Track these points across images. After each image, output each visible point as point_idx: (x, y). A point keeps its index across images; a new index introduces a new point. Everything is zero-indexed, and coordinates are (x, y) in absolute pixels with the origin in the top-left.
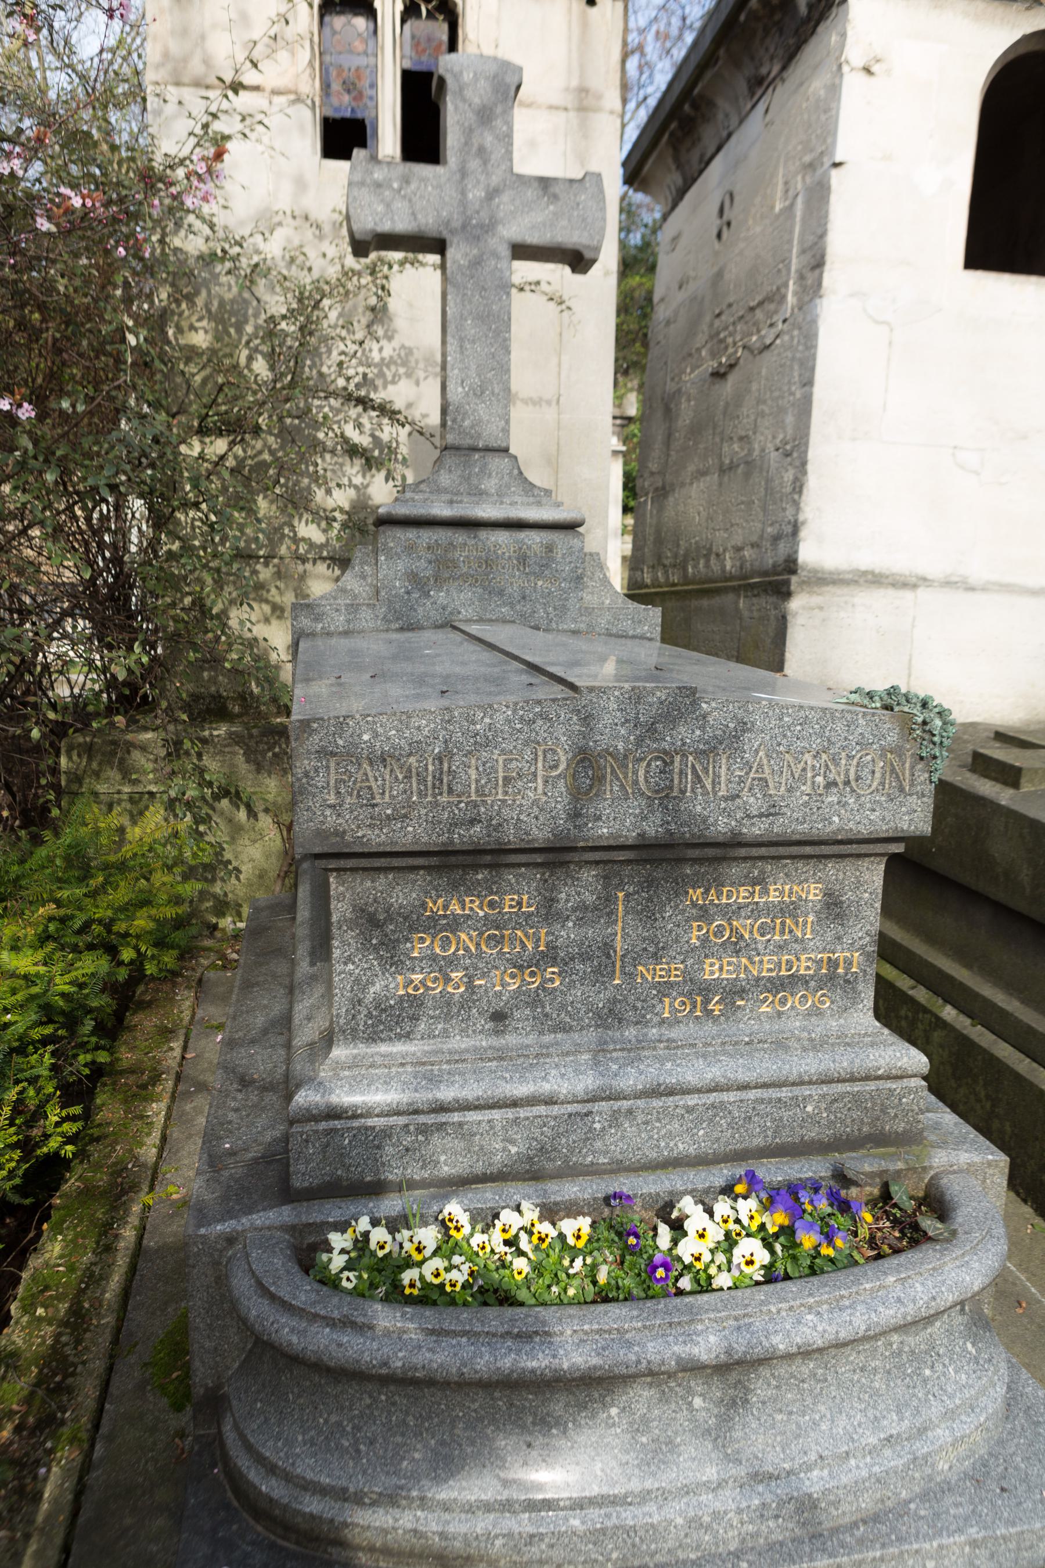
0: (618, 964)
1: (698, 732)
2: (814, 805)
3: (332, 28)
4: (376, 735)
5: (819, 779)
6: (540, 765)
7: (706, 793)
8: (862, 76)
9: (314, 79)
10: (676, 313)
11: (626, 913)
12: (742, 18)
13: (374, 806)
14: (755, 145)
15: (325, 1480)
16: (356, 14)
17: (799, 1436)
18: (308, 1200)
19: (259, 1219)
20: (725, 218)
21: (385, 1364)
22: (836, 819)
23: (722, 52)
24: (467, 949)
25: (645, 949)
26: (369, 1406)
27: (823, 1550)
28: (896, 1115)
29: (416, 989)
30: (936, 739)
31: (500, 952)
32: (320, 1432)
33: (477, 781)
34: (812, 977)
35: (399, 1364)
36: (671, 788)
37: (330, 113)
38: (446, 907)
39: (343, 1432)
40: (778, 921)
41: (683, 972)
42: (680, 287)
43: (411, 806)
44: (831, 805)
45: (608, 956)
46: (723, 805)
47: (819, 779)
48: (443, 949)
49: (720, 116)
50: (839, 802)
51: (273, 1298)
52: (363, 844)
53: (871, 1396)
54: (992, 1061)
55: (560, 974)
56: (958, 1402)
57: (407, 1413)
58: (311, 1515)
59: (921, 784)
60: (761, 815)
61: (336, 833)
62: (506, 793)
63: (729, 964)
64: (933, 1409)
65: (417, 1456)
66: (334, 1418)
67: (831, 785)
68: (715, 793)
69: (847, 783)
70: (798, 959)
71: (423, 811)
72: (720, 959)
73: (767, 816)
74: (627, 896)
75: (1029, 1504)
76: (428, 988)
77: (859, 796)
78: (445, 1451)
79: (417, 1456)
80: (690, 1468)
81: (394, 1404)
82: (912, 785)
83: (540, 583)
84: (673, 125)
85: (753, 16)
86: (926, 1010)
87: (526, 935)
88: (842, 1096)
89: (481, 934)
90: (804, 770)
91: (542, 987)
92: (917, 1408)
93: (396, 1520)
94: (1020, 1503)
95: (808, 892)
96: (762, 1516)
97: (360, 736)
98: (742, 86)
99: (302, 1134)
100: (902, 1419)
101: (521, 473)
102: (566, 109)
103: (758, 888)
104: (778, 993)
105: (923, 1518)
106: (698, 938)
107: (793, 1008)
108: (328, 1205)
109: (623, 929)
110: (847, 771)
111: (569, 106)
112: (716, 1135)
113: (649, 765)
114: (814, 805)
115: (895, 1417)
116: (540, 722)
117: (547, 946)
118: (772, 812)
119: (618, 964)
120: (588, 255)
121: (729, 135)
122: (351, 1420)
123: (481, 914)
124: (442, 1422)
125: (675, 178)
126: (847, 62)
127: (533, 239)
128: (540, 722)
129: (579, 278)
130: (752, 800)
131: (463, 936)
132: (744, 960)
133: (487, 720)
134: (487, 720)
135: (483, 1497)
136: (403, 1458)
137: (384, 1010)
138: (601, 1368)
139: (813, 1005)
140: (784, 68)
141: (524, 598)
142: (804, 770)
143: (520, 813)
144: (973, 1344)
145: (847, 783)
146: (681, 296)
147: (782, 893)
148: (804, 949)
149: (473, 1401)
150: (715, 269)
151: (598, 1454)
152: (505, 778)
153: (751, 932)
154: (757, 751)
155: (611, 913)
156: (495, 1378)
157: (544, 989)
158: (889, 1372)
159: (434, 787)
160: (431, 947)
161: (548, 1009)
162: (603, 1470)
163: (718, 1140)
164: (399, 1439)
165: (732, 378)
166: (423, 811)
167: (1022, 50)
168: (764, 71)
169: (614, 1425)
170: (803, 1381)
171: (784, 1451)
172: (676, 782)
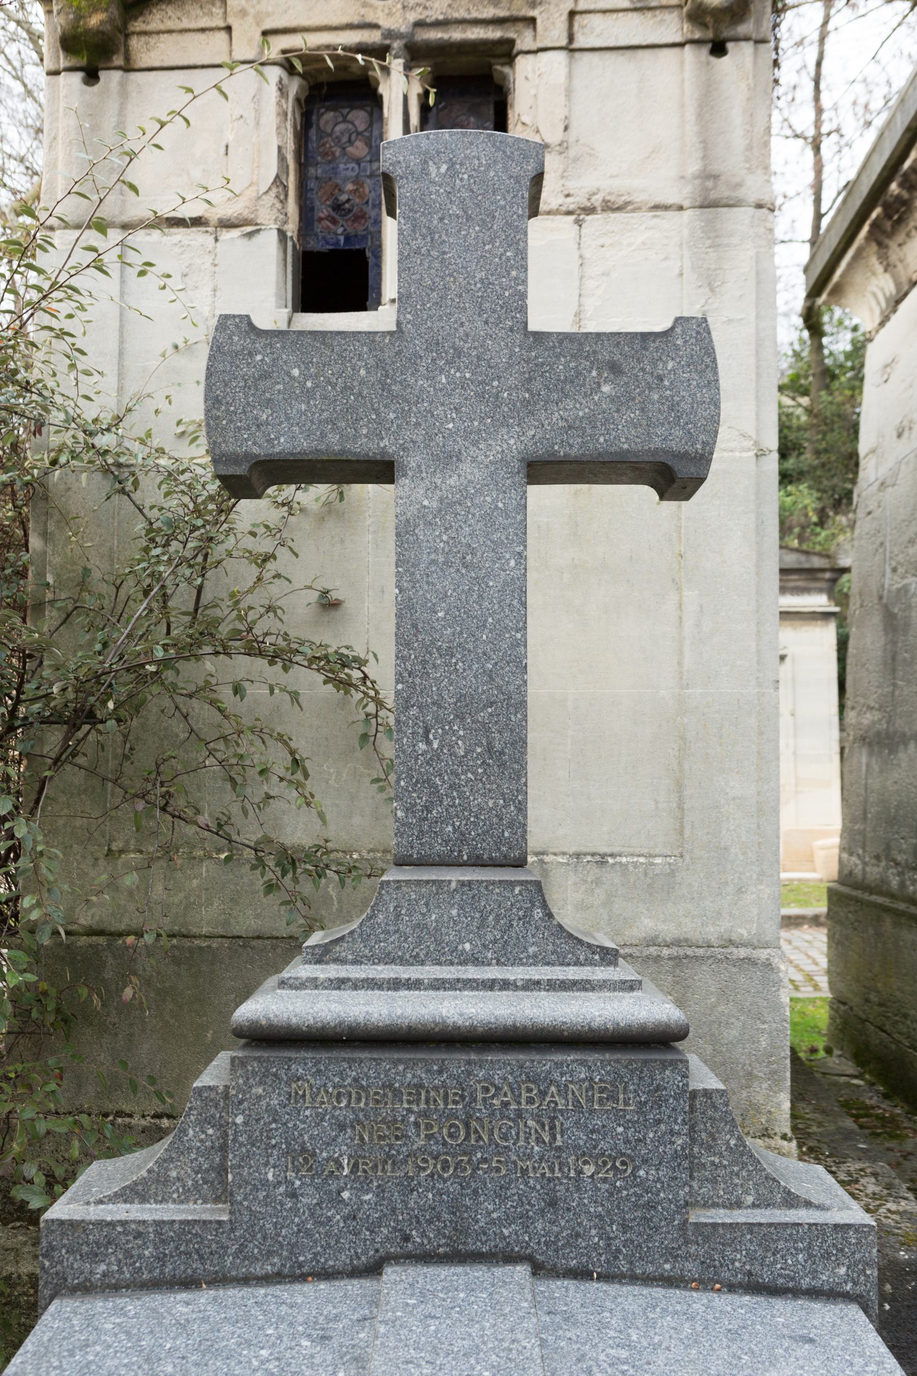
3: (318, 128)
9: (284, 202)
10: (895, 473)
16: (352, 108)
37: (315, 245)
42: (899, 436)
83: (589, 1170)
84: (876, 212)
101: (550, 916)
111: (686, 204)
120: (683, 470)
141: (553, 1203)
146: (902, 448)
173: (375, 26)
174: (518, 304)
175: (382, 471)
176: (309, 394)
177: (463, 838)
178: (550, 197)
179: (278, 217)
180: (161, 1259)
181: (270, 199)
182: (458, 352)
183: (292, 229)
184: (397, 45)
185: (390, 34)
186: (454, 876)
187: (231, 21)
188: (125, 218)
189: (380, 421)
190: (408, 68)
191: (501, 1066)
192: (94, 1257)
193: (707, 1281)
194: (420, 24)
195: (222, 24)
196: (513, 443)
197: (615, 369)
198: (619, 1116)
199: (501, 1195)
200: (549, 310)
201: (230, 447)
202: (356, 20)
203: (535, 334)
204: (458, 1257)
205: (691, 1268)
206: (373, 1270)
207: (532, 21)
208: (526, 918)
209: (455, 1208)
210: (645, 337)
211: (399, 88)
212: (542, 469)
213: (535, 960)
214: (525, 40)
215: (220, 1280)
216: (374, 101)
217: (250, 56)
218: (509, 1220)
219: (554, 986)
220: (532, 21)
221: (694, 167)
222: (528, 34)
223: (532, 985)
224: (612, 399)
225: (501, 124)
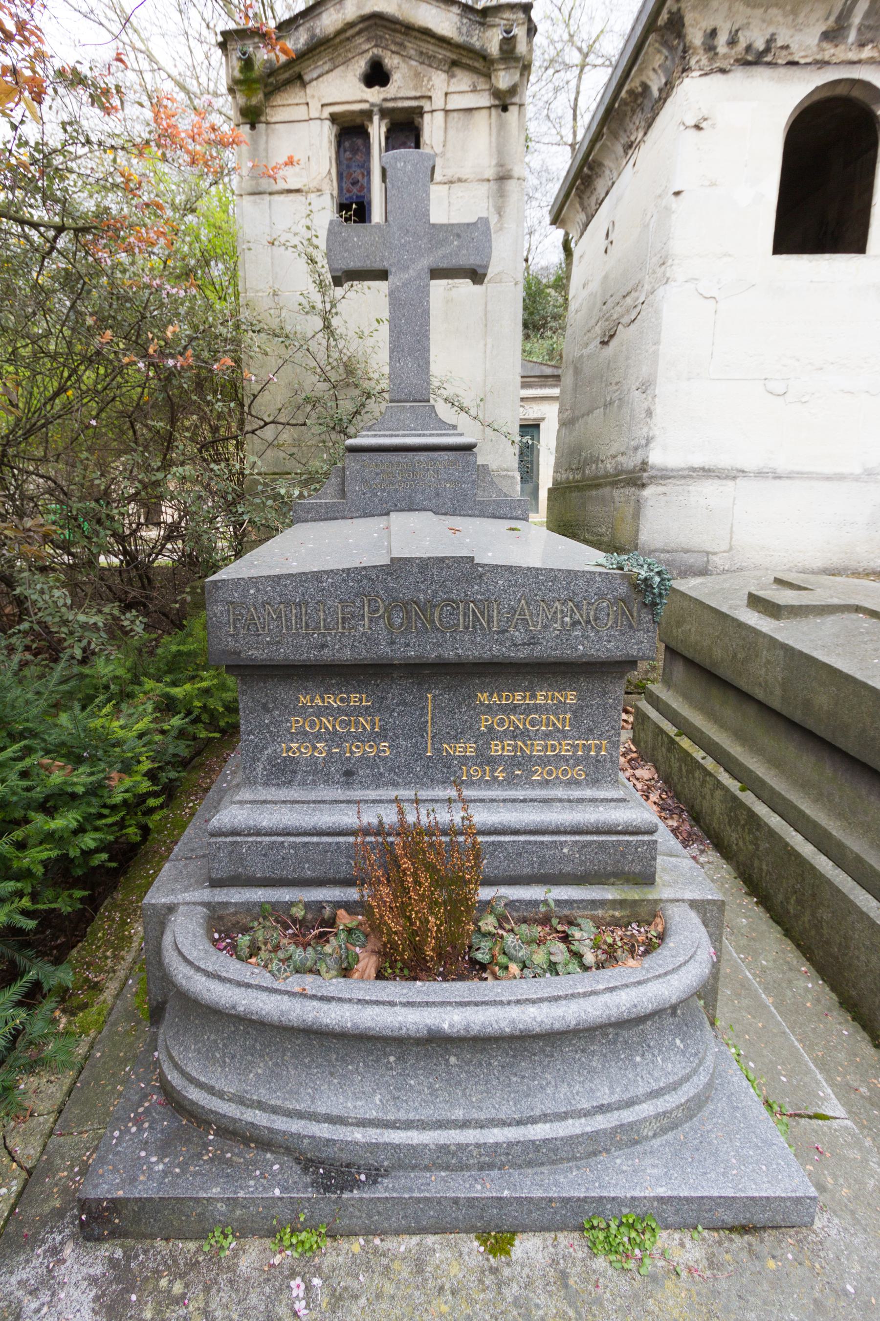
0: (430, 742)
1: (476, 587)
2: (564, 638)
4: (258, 590)
5: (567, 619)
6: (366, 609)
7: (483, 629)
8: (693, 132)
10: (581, 305)
11: (434, 708)
12: (616, 105)
13: (259, 635)
14: (629, 187)
15: (203, 1079)
17: (529, 1095)
18: (221, 887)
19: (188, 897)
20: (610, 239)
21: (234, 1007)
22: (581, 647)
23: (605, 130)
24: (326, 728)
25: (448, 733)
26: (233, 1032)
27: (540, 1186)
28: (633, 860)
29: (294, 753)
30: (656, 591)
31: (348, 731)
32: (204, 1045)
33: (325, 620)
34: (571, 757)
35: (242, 1009)
36: (458, 625)
38: (312, 701)
39: (218, 1049)
40: (544, 717)
41: (476, 750)
43: (282, 636)
44: (576, 637)
45: (423, 737)
46: (496, 637)
47: (567, 619)
48: (311, 728)
49: (607, 172)
50: (582, 636)
51: (180, 953)
52: (252, 660)
53: (589, 1072)
54: (752, 816)
55: (389, 747)
56: (662, 1085)
57: (256, 1041)
58: (192, 1100)
59: (646, 623)
60: (524, 644)
61: (235, 653)
62: (344, 628)
63: (509, 745)
64: (640, 1089)
65: (259, 1071)
66: (213, 1037)
67: (575, 623)
68: (490, 629)
69: (588, 622)
70: (560, 744)
71: (290, 639)
72: (502, 742)
73: (529, 645)
74: (434, 697)
75: (713, 1175)
76: (302, 753)
77: (598, 631)
78: (278, 1070)
79: (259, 1071)
80: (443, 1108)
81: (248, 1033)
82: (639, 623)
85: (624, 103)
86: (710, 774)
87: (366, 721)
88: (591, 843)
89: (335, 719)
90: (555, 613)
91: (377, 755)
92: (626, 1086)
93: (242, 1114)
94: (706, 1173)
95: (566, 698)
96: (496, 1152)
97: (248, 591)
98: (619, 149)
99: (216, 843)
100: (612, 1093)
102: (489, 180)
103: (528, 694)
104: (546, 766)
105: (624, 1172)
106: (486, 726)
107: (557, 777)
108: (233, 890)
109: (432, 719)
110: (588, 614)
112: (496, 864)
113: (442, 609)
114: (564, 638)
115: (607, 1091)
116: (365, 581)
117: (380, 728)
118: (533, 642)
119: (430, 742)
120: (480, 271)
121: (613, 183)
122: (222, 1040)
123: (335, 705)
124: (277, 1050)
125: (582, 217)
126: (521, 105)
127: (444, 264)
128: (365, 581)
129: (477, 287)
130: (517, 633)
131: (324, 720)
132: (520, 743)
133: (330, 580)
134: (330, 580)
135: (298, 1107)
136: (251, 1072)
137: (274, 766)
138: (374, 1029)
139: (573, 776)
140: (645, 134)
142: (555, 613)
143: (354, 641)
144: (682, 1041)
145: (588, 622)
147: (546, 697)
148: (565, 738)
149: (297, 1039)
150: (604, 273)
151: (379, 1089)
152: (343, 618)
153: (524, 724)
154: (520, 600)
155: (424, 708)
156: (302, 1026)
157: (379, 757)
158: (605, 1056)
159: (296, 623)
160: (303, 726)
161: (382, 770)
162: (381, 1101)
163: (497, 867)
164: (249, 1058)
165: (614, 343)
166: (290, 639)
167: (816, 98)
168: (633, 138)
169: (391, 1069)
170: (535, 1055)
171: (515, 1104)
172: (461, 621)
173: (366, 101)
174: (426, 214)
175: (382, 275)
176: (360, 247)
177: (410, 393)
178: (438, 177)
179: (331, 188)
180: (327, 513)
181: (327, 180)
182: (408, 231)
183: (335, 193)
184: (376, 109)
185: (372, 105)
186: (408, 404)
187: (309, 100)
188: (270, 190)
189: (383, 256)
190: (381, 119)
191: (423, 456)
192: (308, 512)
193: (482, 515)
194: (385, 100)
195: (304, 101)
196: (426, 262)
197: (458, 236)
198: (457, 470)
199: (423, 492)
200: (438, 215)
201: (336, 266)
202: (359, 98)
203: (434, 225)
204: (410, 510)
205: (477, 512)
206: (388, 514)
207: (430, 98)
208: (430, 417)
209: (410, 497)
210: (468, 224)
211: (377, 130)
212: (437, 273)
213: (433, 429)
214: (427, 108)
215: (343, 518)
216: (366, 135)
217: (317, 116)
218: (425, 500)
219: (438, 435)
220: (430, 98)
221: (494, 162)
222: (428, 103)
223: (432, 435)
224: (458, 247)
225: (417, 146)
